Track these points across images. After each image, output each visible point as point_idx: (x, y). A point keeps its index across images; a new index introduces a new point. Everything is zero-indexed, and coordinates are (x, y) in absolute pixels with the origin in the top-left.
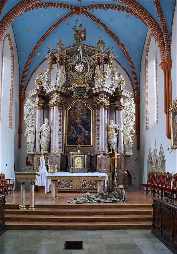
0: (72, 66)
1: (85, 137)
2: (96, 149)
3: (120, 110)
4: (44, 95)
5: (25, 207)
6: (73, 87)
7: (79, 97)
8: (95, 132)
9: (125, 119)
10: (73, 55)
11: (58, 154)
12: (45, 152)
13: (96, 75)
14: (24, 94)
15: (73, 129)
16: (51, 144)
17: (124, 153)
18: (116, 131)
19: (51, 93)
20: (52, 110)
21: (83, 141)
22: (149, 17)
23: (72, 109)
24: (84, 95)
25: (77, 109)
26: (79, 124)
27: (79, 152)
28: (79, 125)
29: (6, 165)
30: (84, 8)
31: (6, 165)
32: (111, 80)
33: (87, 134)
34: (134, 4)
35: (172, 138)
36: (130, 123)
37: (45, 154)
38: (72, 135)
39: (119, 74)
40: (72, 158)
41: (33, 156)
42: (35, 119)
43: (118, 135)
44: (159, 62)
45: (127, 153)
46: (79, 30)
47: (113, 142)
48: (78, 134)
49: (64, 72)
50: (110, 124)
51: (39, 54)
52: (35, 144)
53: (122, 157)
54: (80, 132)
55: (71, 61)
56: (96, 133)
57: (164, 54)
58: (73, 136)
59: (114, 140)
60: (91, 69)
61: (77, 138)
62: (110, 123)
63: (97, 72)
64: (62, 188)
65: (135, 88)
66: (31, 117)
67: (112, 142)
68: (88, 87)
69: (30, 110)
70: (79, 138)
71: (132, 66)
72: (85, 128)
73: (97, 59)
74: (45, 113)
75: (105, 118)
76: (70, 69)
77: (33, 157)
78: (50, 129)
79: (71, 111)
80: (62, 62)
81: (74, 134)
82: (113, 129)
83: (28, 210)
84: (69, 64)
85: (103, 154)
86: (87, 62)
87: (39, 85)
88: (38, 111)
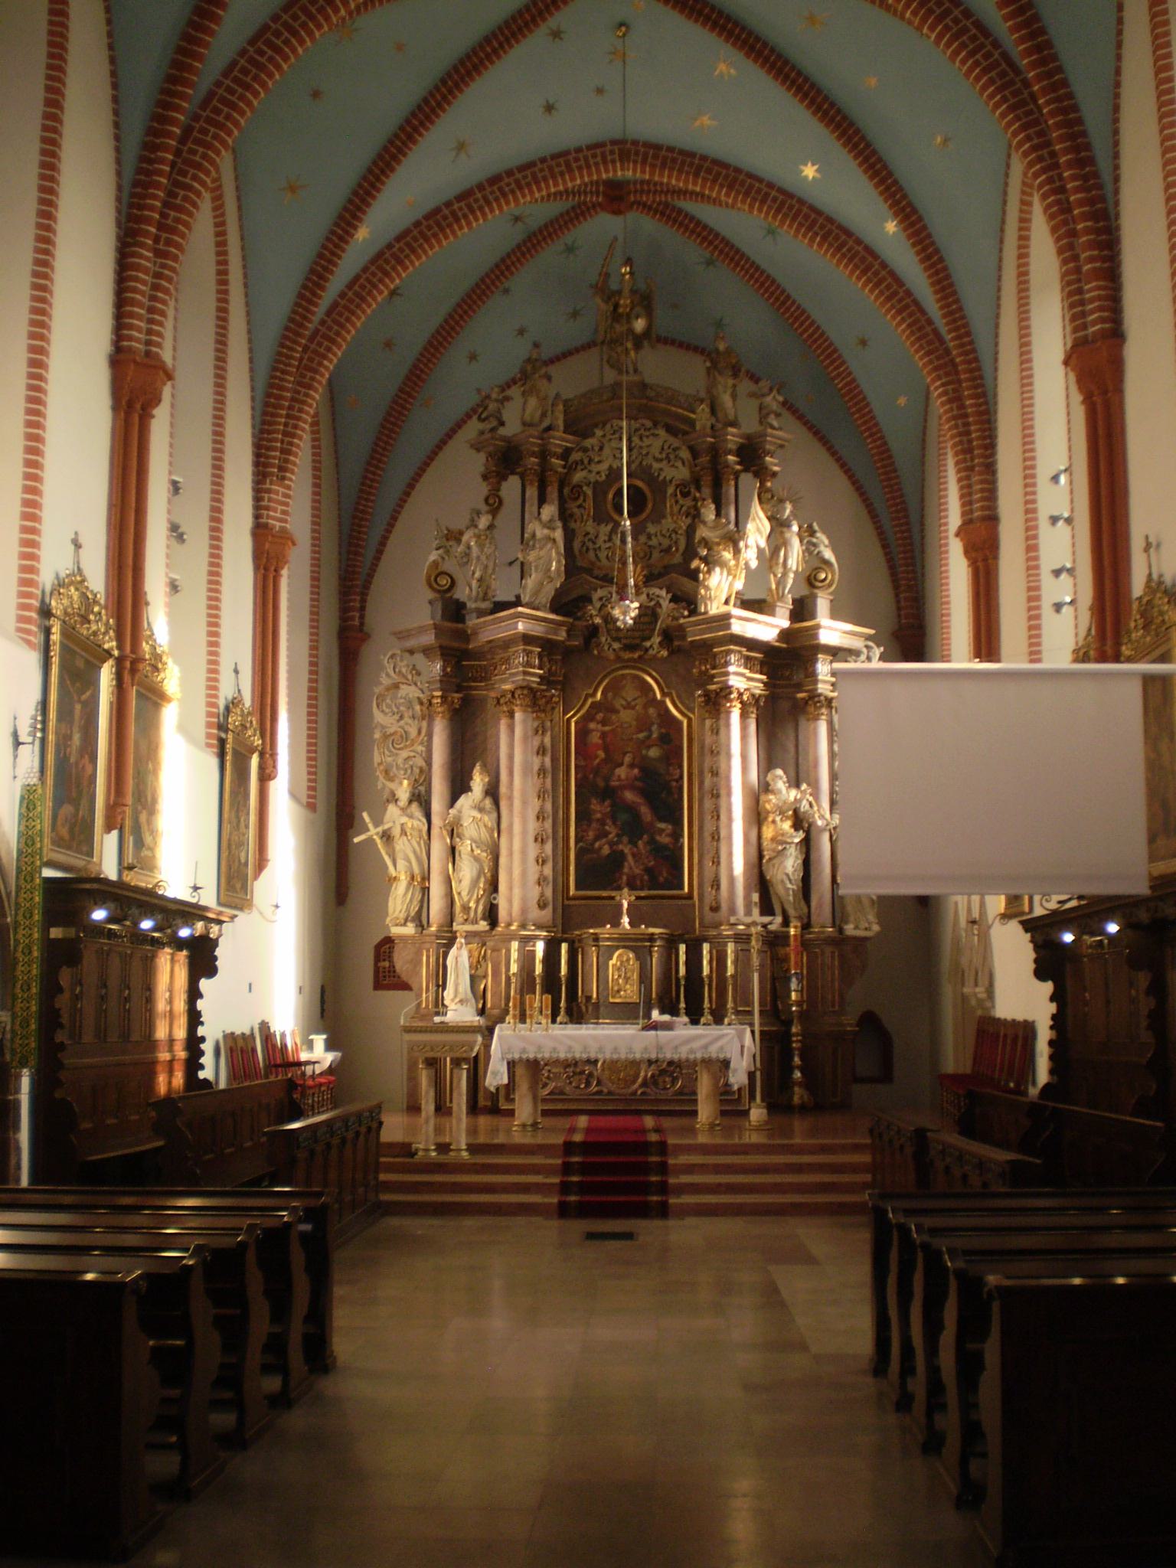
0: (589, 492)
1: (657, 849)
4: (464, 646)
5: (435, 1150)
7: (627, 655)
8: (701, 828)
10: (596, 426)
14: (362, 617)
15: (599, 816)
17: (841, 930)
19: (507, 643)
21: (648, 870)
23: (594, 712)
24: (648, 644)
28: (629, 796)
29: (250, 985)
31: (250, 985)
33: (664, 839)
37: (470, 936)
38: (597, 845)
39: (810, 527)
40: (595, 955)
45: (850, 929)
46: (619, 292)
47: (785, 877)
49: (559, 534)
52: (425, 891)
53: (828, 950)
55: (586, 461)
58: (600, 848)
59: (791, 863)
60: (681, 502)
62: (767, 785)
63: (702, 532)
64: (555, 1094)
68: (665, 604)
70: (630, 858)
71: (884, 453)
72: (654, 808)
76: (579, 506)
79: (592, 726)
80: (543, 471)
81: (604, 840)
83: (443, 1158)
84: (578, 476)
87: (439, 591)
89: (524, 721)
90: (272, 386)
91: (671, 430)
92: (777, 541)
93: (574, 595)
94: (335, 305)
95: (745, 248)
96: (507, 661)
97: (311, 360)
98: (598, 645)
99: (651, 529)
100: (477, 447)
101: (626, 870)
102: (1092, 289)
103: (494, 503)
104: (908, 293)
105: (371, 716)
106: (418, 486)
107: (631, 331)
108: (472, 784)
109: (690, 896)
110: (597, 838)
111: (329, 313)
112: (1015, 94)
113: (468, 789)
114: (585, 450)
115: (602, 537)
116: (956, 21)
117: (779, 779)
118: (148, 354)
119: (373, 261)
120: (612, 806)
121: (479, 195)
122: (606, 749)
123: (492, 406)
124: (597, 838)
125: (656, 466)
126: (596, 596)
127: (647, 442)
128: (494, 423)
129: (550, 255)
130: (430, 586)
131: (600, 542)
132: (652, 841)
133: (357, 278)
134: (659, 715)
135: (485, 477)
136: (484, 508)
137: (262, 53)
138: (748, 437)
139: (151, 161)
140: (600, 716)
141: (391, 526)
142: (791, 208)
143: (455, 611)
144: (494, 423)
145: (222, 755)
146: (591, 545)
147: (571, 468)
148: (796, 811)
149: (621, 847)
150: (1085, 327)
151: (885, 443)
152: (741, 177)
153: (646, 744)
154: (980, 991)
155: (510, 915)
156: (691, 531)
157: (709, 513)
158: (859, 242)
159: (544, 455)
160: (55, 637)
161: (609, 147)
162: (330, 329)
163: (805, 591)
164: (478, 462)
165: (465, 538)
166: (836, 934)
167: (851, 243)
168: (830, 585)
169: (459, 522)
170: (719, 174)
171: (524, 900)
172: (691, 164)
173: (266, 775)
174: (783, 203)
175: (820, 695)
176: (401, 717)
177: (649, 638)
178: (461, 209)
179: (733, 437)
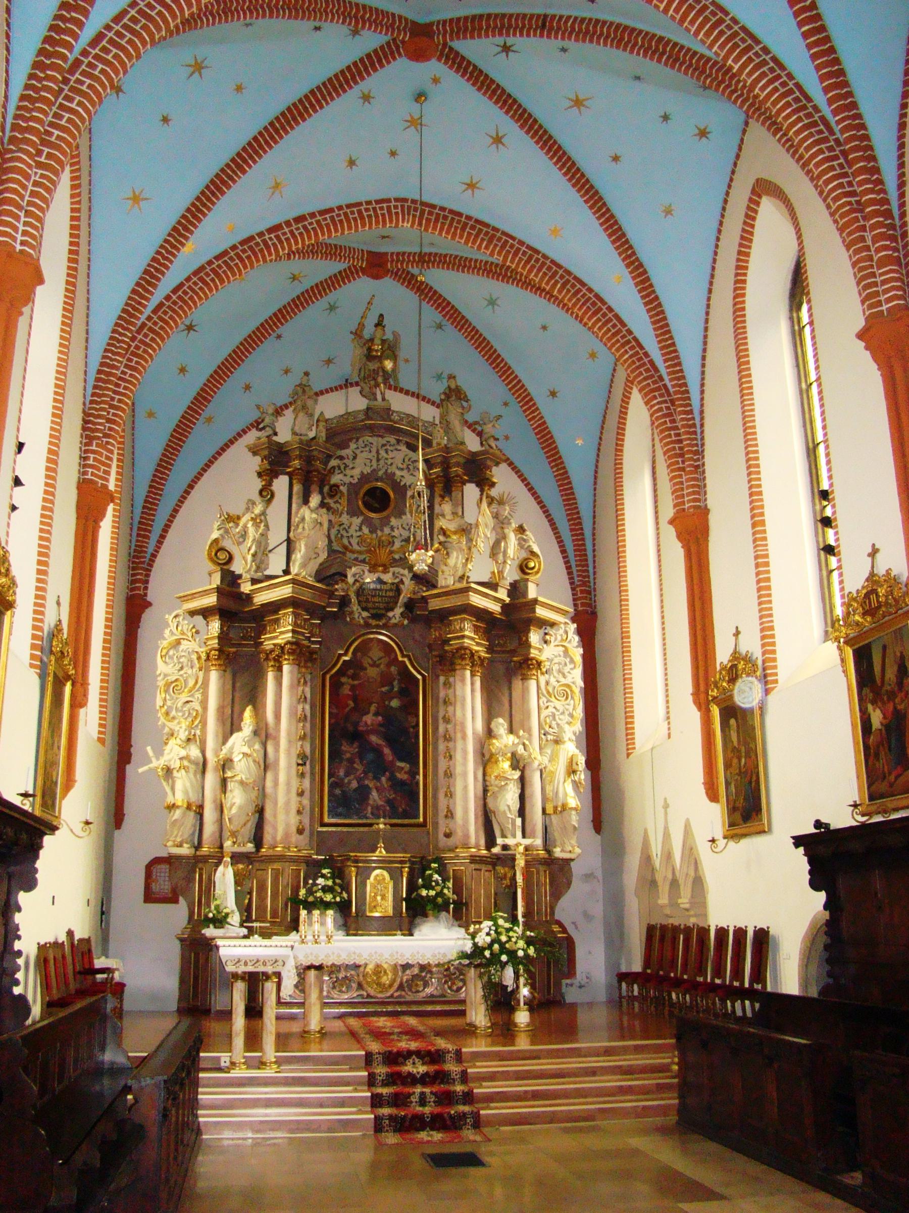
1: (397, 784)
2: (441, 836)
3: (525, 678)
7: (373, 622)
9: (544, 713)
15: (348, 755)
16: (268, 814)
17: (549, 851)
18: (514, 767)
19: (275, 607)
20: (270, 676)
21: (389, 802)
22: (628, 342)
24: (390, 614)
25: (365, 669)
27: (381, 852)
28: (374, 739)
30: (398, 260)
32: (494, 554)
33: (401, 776)
34: (579, 291)
35: (723, 798)
36: (566, 727)
37: (236, 858)
40: (354, 874)
42: (199, 708)
43: (522, 780)
44: (668, 511)
45: (558, 853)
48: (370, 775)
52: (201, 815)
53: (542, 868)
54: (379, 767)
55: (342, 467)
56: (441, 772)
57: (682, 483)
58: (349, 783)
61: (363, 793)
63: (441, 523)
65: (576, 579)
66: (184, 697)
67: (502, 807)
69: (182, 668)
73: (442, 463)
74: (238, 685)
78: (262, 752)
79: (344, 680)
82: (504, 755)
84: (336, 479)
85: (474, 859)
86: (404, 473)
87: (219, 564)
88: (214, 676)
89: (291, 672)
92: (457, 558)
93: (333, 571)
95: (469, 316)
96: (277, 621)
98: (352, 613)
100: (254, 450)
101: (371, 802)
103: (267, 494)
105: (155, 667)
106: (197, 487)
107: (383, 369)
108: (242, 724)
109: (424, 825)
111: (155, 311)
113: (239, 729)
114: (341, 458)
115: (354, 527)
116: (757, 55)
117: (500, 725)
120: (360, 747)
121: (286, 230)
122: (355, 701)
123: (267, 420)
124: (347, 774)
126: (350, 573)
127: (391, 455)
128: (269, 431)
129: (315, 312)
130: (211, 559)
131: (352, 531)
133: (181, 285)
134: (399, 674)
135: (260, 475)
140: (351, 672)
141: (173, 516)
142: (537, 260)
145: (43, 676)
146: (345, 534)
148: (514, 755)
149: (366, 782)
151: (566, 472)
152: (499, 235)
153: (389, 696)
155: (274, 838)
158: (590, 290)
161: (393, 203)
162: (155, 323)
164: (256, 463)
166: (547, 856)
167: (584, 290)
168: (537, 572)
170: (480, 230)
171: (288, 825)
172: (459, 222)
173: (78, 702)
174: (531, 257)
175: (532, 659)
176: (182, 668)
177: (392, 609)
178: (271, 239)
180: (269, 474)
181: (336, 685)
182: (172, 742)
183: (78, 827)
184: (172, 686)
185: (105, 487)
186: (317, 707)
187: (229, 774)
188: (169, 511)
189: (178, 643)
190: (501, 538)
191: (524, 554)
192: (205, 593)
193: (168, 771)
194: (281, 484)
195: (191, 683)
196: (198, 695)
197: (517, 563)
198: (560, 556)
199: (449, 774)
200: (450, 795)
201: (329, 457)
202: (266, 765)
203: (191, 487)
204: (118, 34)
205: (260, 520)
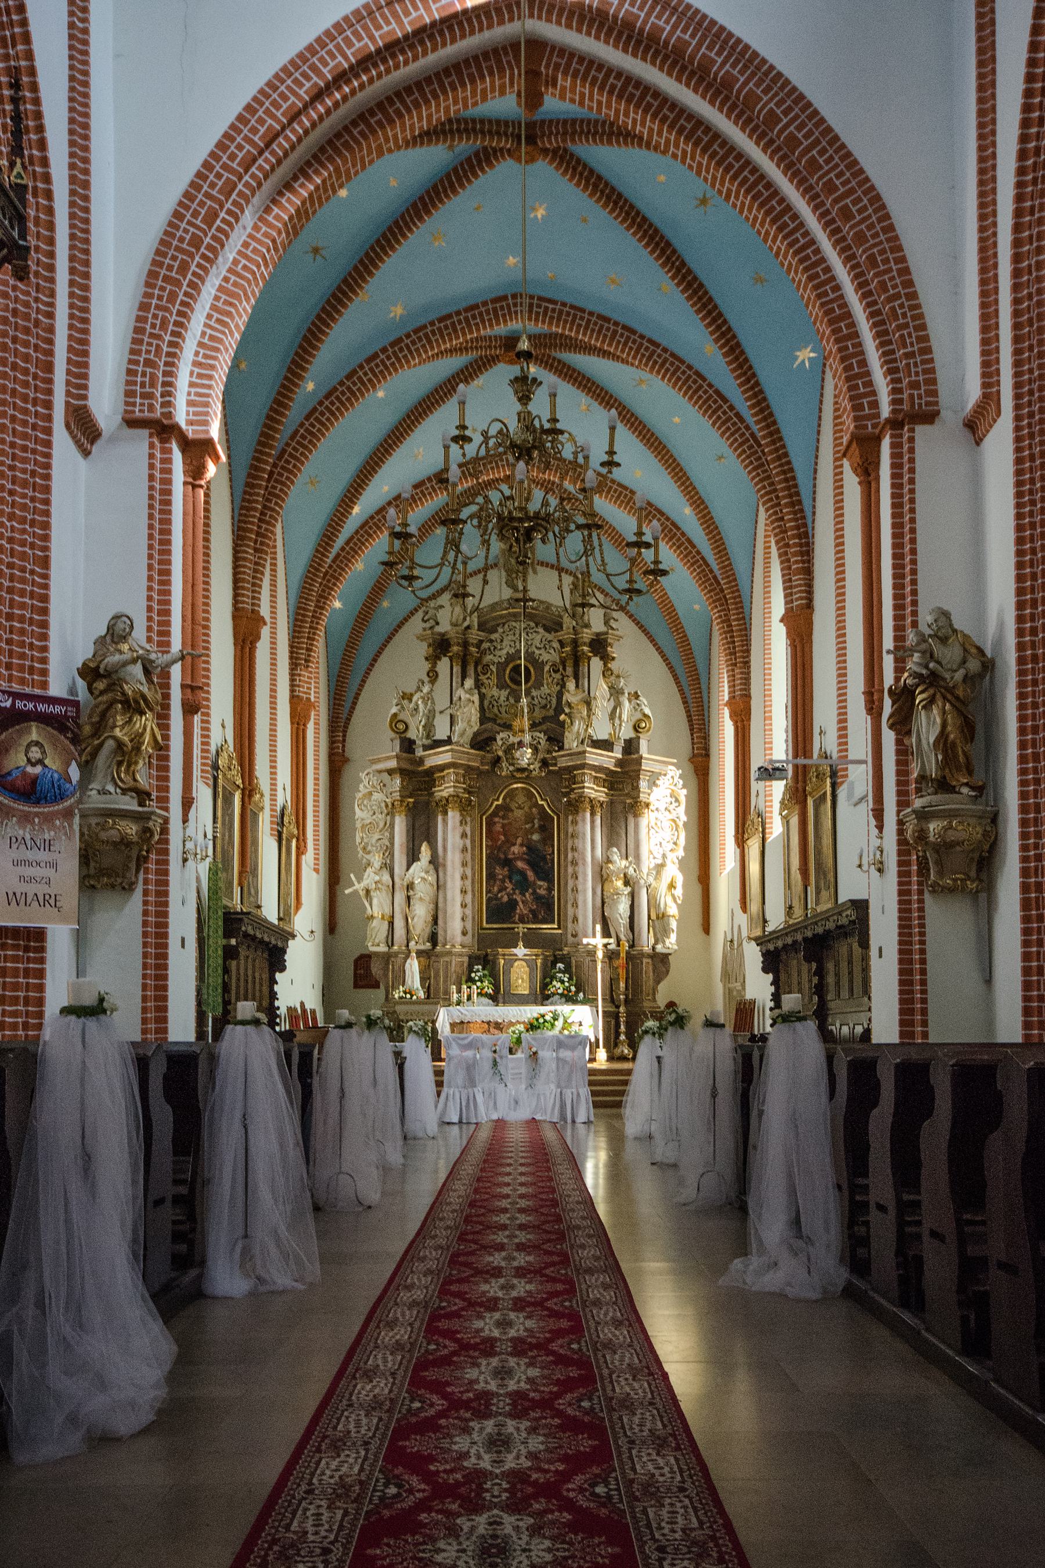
1: (538, 898)
3: (636, 816)
6: (500, 743)
7: (518, 775)
11: (461, 955)
12: (422, 947)
13: (567, 710)
18: (627, 883)
19: (442, 768)
20: (440, 818)
21: (531, 911)
26: (518, 859)
32: (612, 716)
37: (420, 953)
41: (387, 958)
49: (476, 698)
50: (609, 861)
51: (385, 604)
52: (391, 924)
59: (623, 907)
61: (512, 904)
63: (567, 697)
66: (377, 836)
71: (684, 641)
72: (536, 873)
75: (593, 841)
77: (387, 964)
80: (465, 655)
84: (488, 658)
86: (542, 651)
90: (299, 608)
91: (547, 629)
94: (338, 555)
97: (323, 591)
99: (534, 693)
100: (421, 638)
102: (797, 579)
103: (433, 676)
104: (698, 553)
110: (500, 891)
111: (334, 561)
112: (757, 460)
114: (491, 641)
115: (502, 698)
118: (253, 611)
119: (362, 527)
122: (505, 835)
124: (500, 891)
125: (537, 652)
126: (498, 738)
132: (534, 893)
135: (427, 659)
136: (426, 679)
137: (314, 426)
138: (598, 634)
139: (251, 494)
141: (362, 686)
143: (408, 746)
144: (432, 622)
147: (483, 653)
150: (792, 601)
154: (739, 987)
156: (560, 695)
157: (571, 685)
159: (465, 644)
160: (220, 781)
163: (632, 734)
164: (423, 649)
165: (415, 699)
169: (410, 689)
179: (587, 635)
180: (433, 659)
181: (490, 824)
182: (369, 870)
183: (307, 936)
184: (368, 828)
185: (309, 699)
186: (476, 844)
187: (411, 893)
188: (358, 681)
189: (370, 794)
190: (618, 704)
191: (639, 716)
192: (388, 758)
193: (368, 892)
194: (444, 665)
195: (381, 825)
196: (387, 834)
197: (631, 724)
198: (682, 707)
199: (575, 890)
200: (575, 905)
201: (481, 642)
202: (439, 886)
203: (375, 660)
204: (294, 449)
205: (428, 698)
